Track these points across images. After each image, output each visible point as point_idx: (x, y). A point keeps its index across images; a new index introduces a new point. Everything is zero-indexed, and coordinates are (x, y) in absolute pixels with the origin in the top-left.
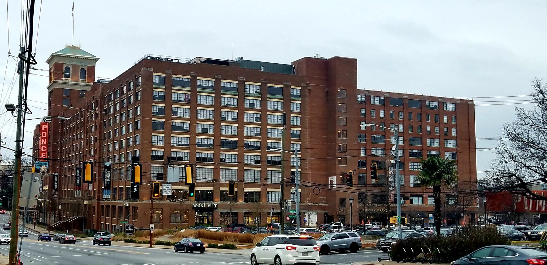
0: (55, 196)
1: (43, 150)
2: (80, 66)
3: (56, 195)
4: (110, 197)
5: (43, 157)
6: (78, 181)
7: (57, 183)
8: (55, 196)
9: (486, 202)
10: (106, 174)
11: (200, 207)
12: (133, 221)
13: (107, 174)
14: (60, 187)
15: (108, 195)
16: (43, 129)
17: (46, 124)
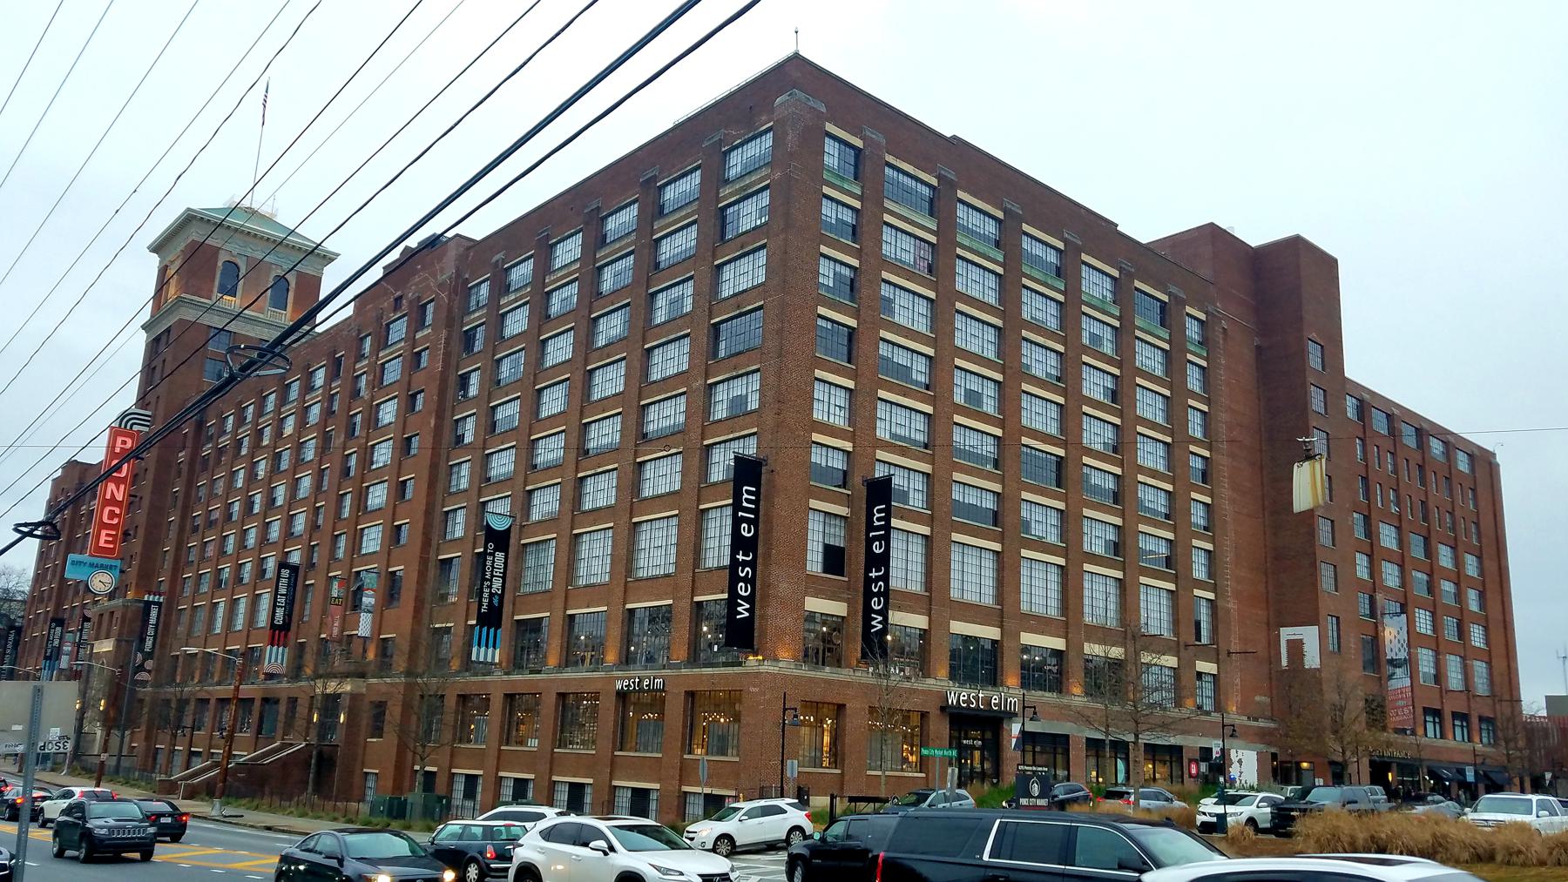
0: (143, 676)
2: (274, 267)
3: (145, 670)
4: (497, 660)
5: (106, 542)
6: (280, 612)
7: (156, 632)
8: (143, 676)
10: (489, 563)
11: (968, 708)
13: (494, 562)
15: (483, 649)
16: (117, 450)
17: (131, 436)
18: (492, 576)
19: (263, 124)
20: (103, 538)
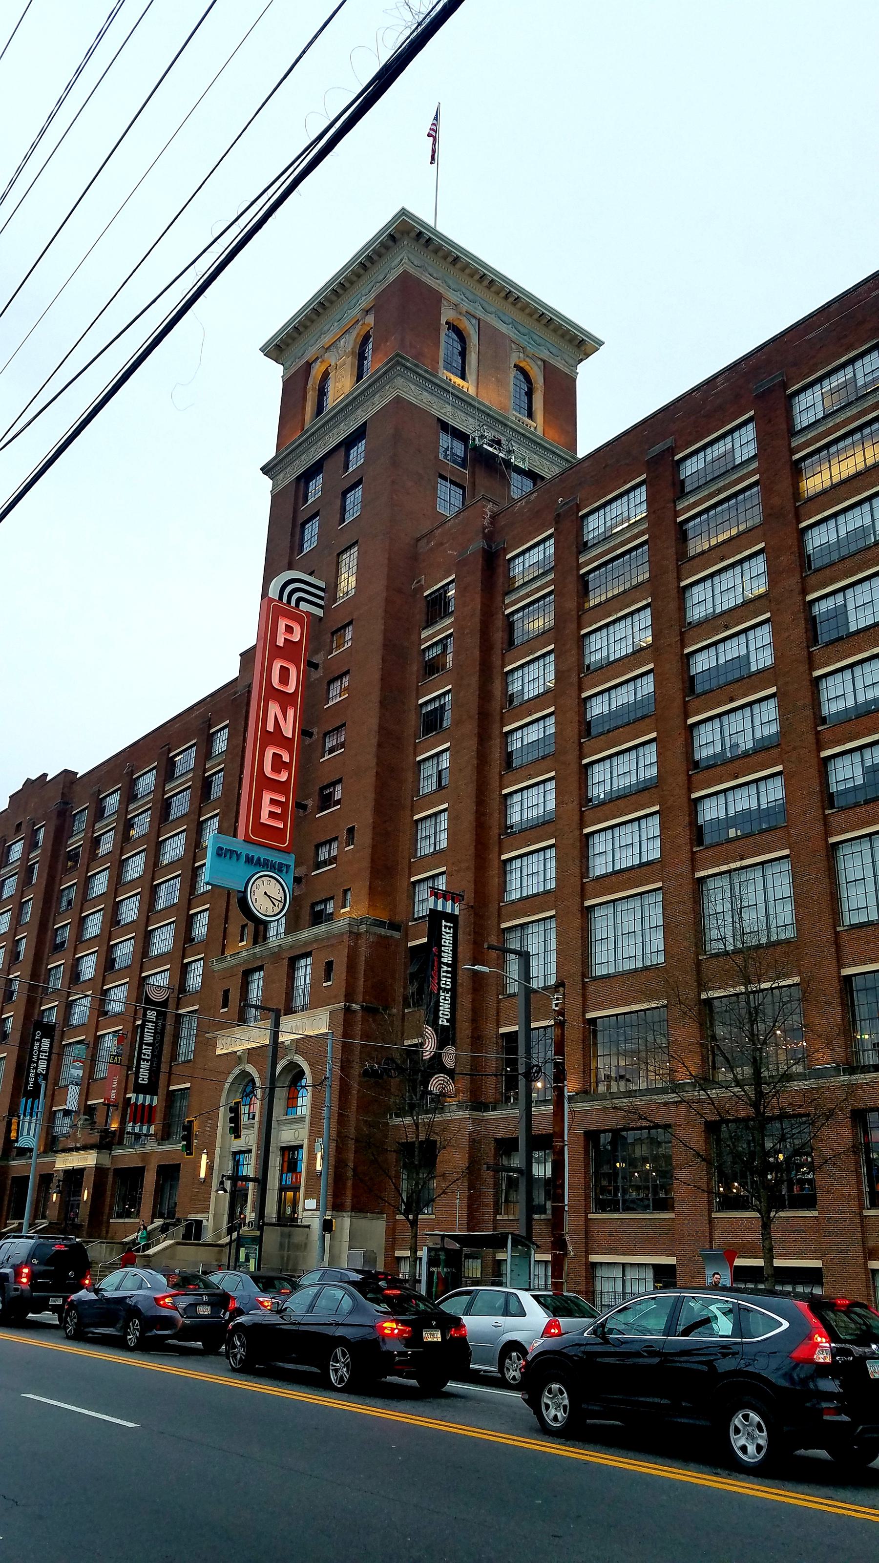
1: (276, 768)
3: (443, 1069)
9: (426, 1083)
10: (36, 1048)
12: (590, 1216)
13: (40, 1047)
14: (477, 1016)
16: (280, 642)
17: (298, 619)
18: (39, 1059)
19: (433, 134)
20: (266, 808)
